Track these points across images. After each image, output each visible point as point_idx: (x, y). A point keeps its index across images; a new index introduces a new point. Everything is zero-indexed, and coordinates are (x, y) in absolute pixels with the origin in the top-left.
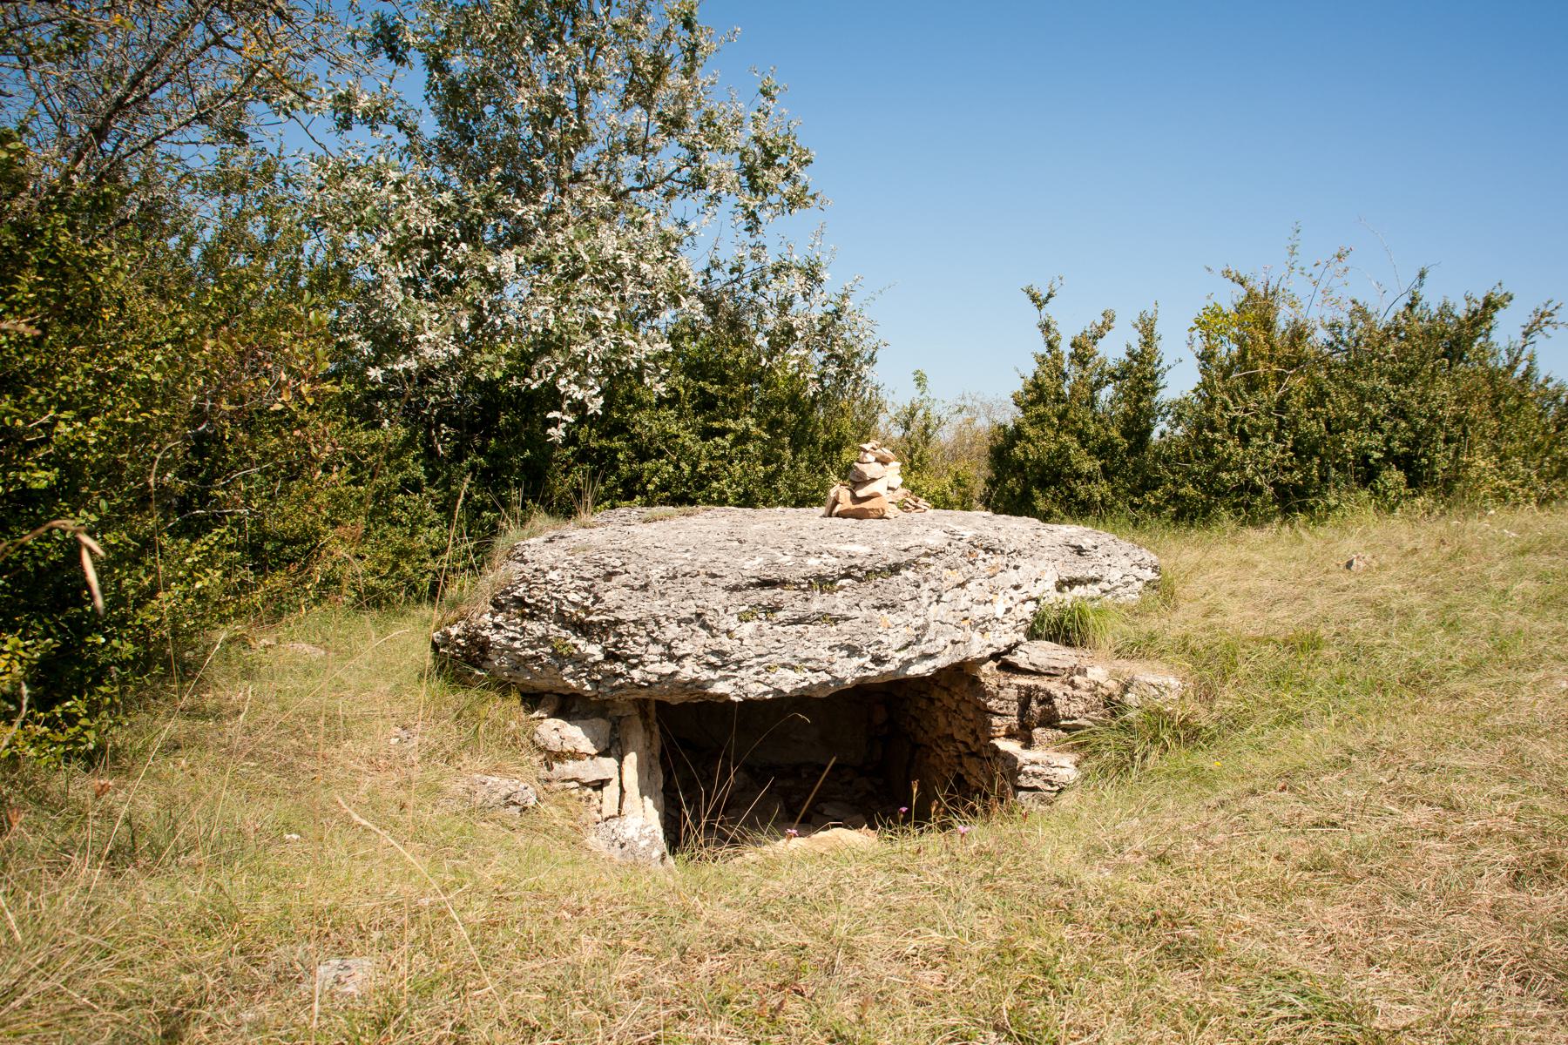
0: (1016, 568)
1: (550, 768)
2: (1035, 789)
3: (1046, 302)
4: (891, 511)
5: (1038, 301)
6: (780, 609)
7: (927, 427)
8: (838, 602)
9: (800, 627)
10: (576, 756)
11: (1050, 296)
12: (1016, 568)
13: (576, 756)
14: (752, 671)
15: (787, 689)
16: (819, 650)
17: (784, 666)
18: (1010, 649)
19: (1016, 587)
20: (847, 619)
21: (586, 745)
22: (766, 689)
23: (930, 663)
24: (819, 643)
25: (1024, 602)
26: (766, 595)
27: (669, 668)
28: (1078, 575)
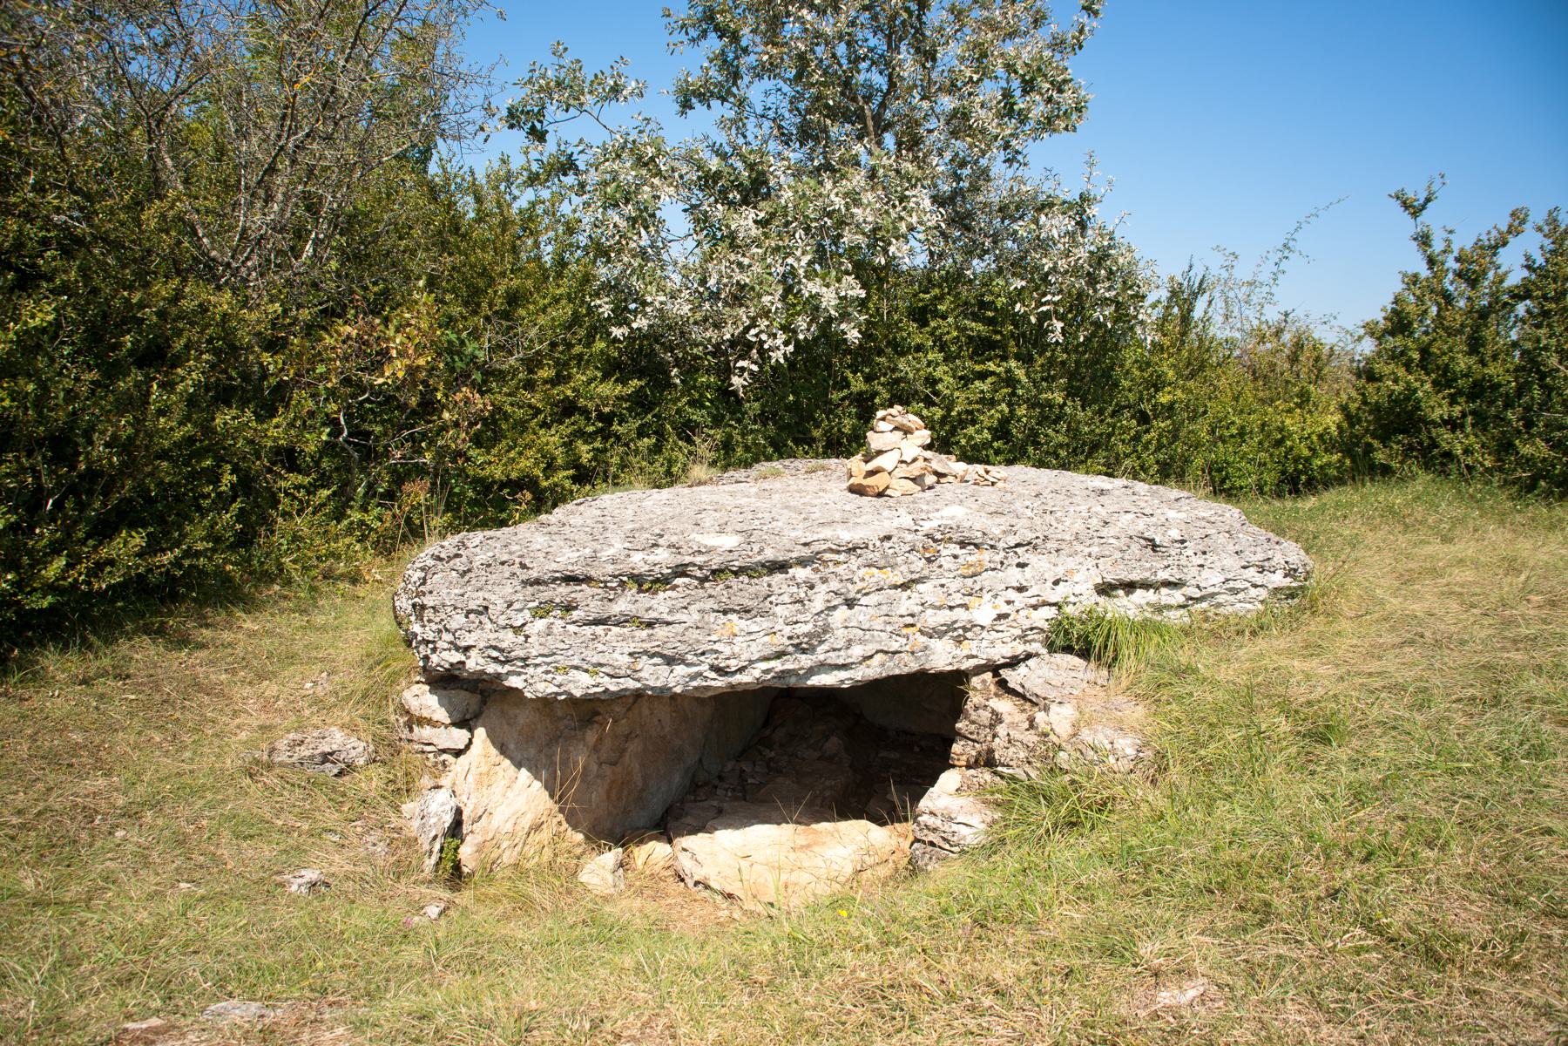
0: (1021, 565)
1: (411, 730)
2: (932, 844)
3: (1424, 207)
4: (899, 486)
5: (1414, 209)
6: (576, 608)
7: (1317, 359)
8: (660, 604)
9: (600, 629)
10: (433, 723)
11: (1428, 200)
12: (1021, 565)
13: (433, 723)
14: (540, 670)
15: (578, 693)
16: (616, 655)
17: (577, 668)
18: (1014, 662)
19: (1021, 589)
20: (668, 624)
21: (441, 715)
22: (556, 689)
23: (843, 675)
24: (617, 648)
25: (1035, 607)
26: (562, 592)
27: (456, 657)
28: (1135, 576)
